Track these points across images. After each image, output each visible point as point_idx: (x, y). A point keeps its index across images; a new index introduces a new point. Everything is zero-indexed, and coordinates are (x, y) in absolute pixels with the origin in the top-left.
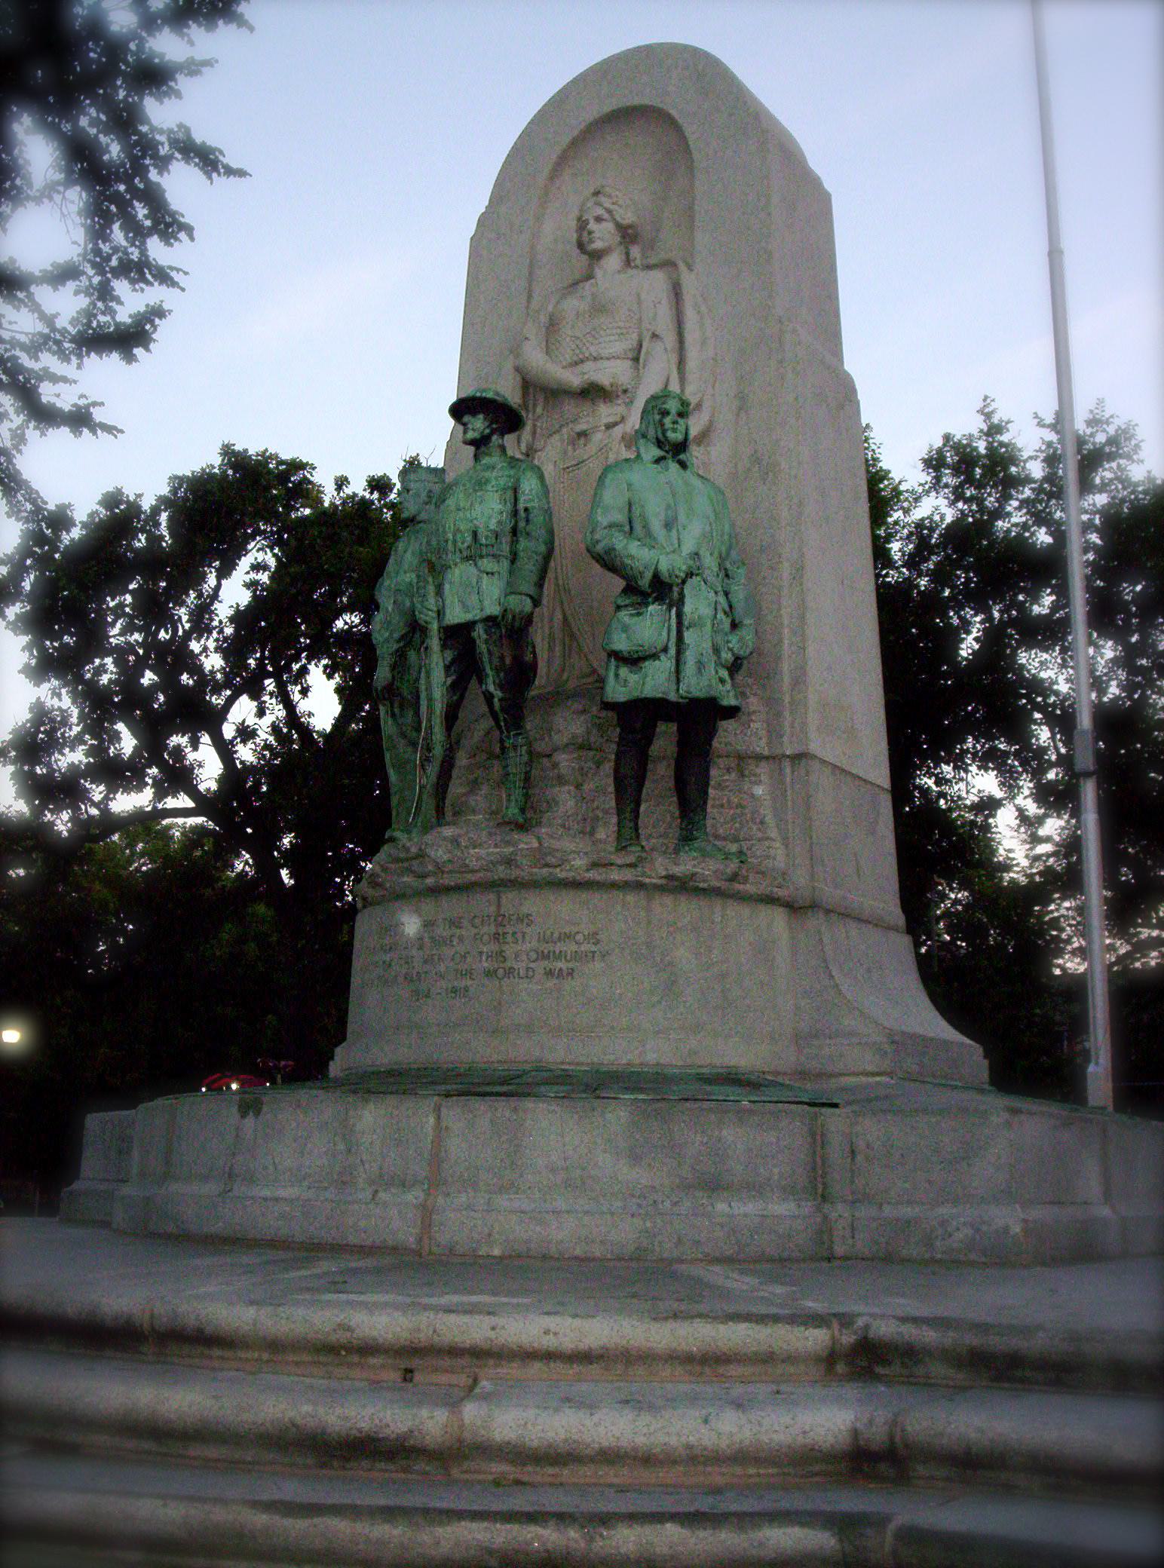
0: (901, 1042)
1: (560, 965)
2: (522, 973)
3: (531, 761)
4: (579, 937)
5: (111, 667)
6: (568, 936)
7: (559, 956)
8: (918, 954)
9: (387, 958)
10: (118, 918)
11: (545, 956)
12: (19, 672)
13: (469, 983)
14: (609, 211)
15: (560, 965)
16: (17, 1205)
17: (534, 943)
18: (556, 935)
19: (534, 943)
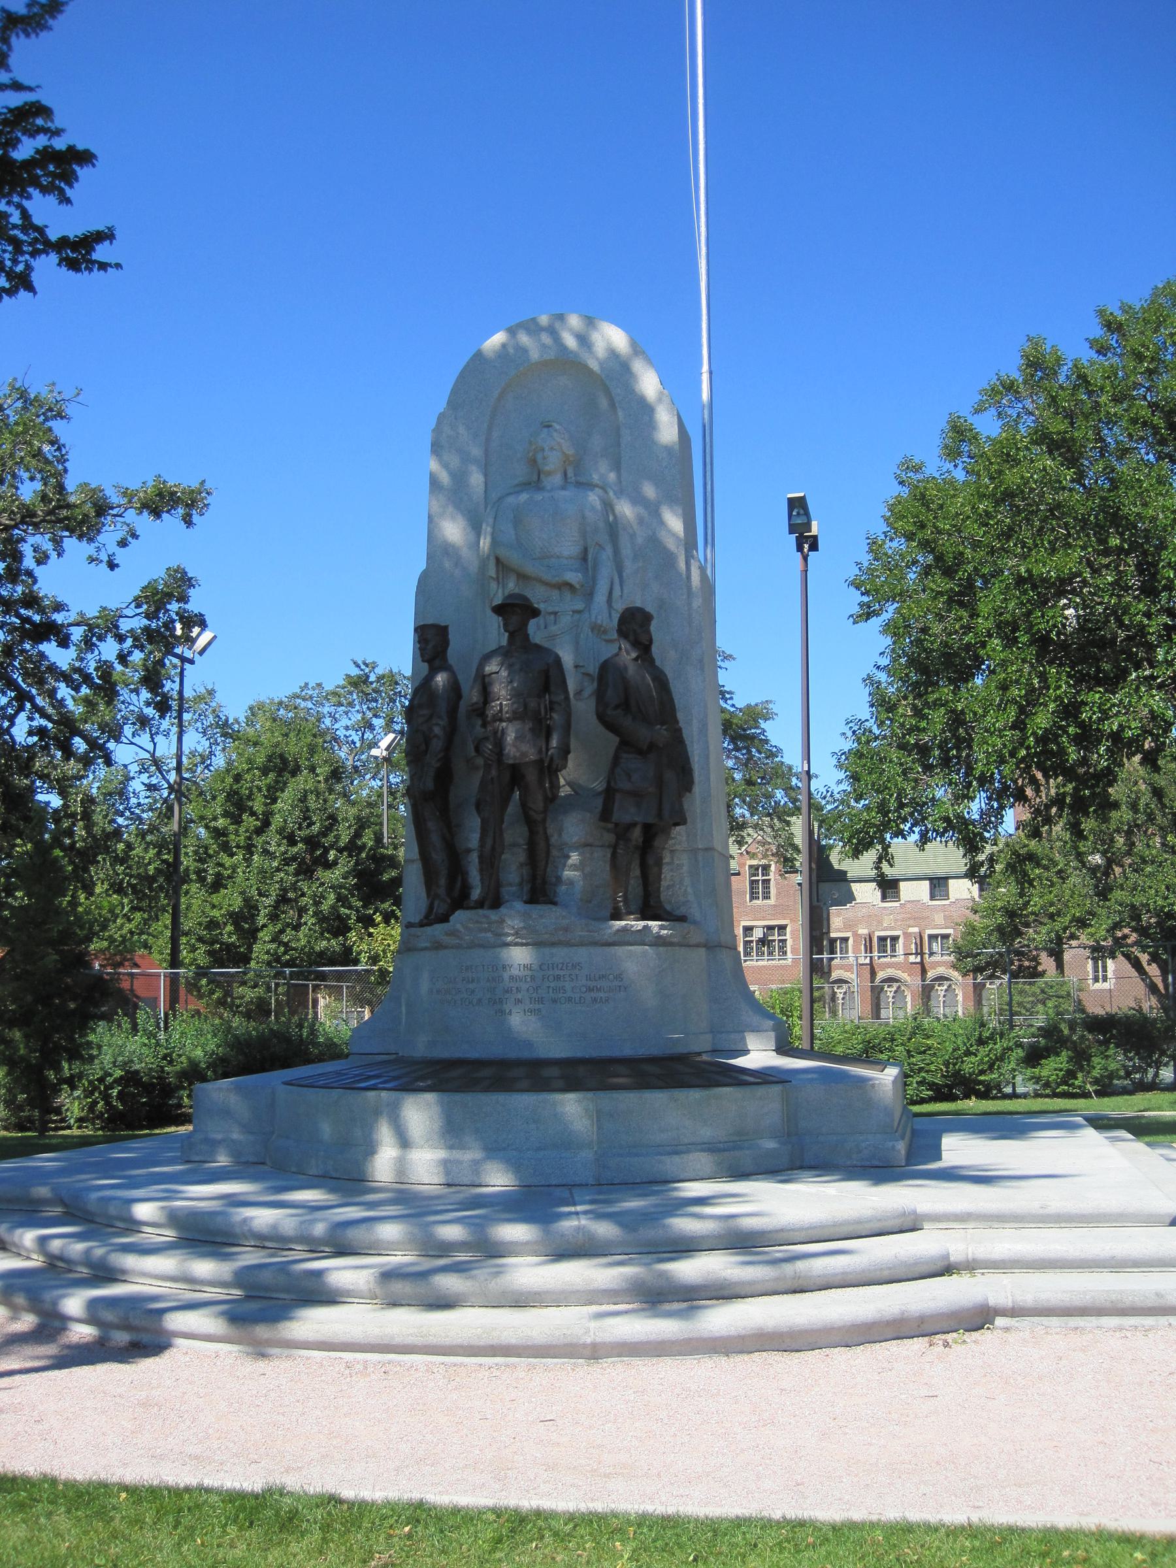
0: (746, 1052)
1: (602, 995)
2: (577, 999)
3: (1098, 434)
4: (611, 977)
5: (38, 539)
6: (602, 977)
7: (599, 990)
8: (811, 959)
9: (471, 986)
10: (638, 499)
11: (590, 990)
12: (94, 165)
13: (541, 1006)
14: (559, 444)
15: (602, 995)
16: (1, 1252)
17: (584, 982)
18: (597, 976)
19: (584, 982)
